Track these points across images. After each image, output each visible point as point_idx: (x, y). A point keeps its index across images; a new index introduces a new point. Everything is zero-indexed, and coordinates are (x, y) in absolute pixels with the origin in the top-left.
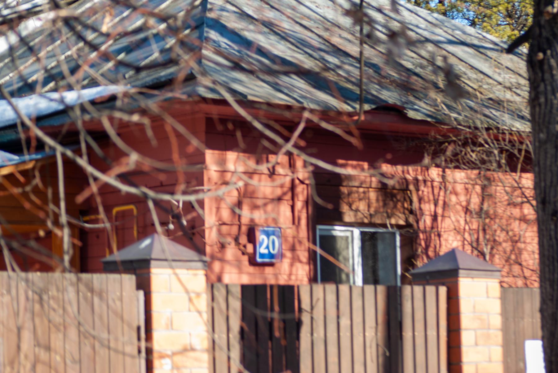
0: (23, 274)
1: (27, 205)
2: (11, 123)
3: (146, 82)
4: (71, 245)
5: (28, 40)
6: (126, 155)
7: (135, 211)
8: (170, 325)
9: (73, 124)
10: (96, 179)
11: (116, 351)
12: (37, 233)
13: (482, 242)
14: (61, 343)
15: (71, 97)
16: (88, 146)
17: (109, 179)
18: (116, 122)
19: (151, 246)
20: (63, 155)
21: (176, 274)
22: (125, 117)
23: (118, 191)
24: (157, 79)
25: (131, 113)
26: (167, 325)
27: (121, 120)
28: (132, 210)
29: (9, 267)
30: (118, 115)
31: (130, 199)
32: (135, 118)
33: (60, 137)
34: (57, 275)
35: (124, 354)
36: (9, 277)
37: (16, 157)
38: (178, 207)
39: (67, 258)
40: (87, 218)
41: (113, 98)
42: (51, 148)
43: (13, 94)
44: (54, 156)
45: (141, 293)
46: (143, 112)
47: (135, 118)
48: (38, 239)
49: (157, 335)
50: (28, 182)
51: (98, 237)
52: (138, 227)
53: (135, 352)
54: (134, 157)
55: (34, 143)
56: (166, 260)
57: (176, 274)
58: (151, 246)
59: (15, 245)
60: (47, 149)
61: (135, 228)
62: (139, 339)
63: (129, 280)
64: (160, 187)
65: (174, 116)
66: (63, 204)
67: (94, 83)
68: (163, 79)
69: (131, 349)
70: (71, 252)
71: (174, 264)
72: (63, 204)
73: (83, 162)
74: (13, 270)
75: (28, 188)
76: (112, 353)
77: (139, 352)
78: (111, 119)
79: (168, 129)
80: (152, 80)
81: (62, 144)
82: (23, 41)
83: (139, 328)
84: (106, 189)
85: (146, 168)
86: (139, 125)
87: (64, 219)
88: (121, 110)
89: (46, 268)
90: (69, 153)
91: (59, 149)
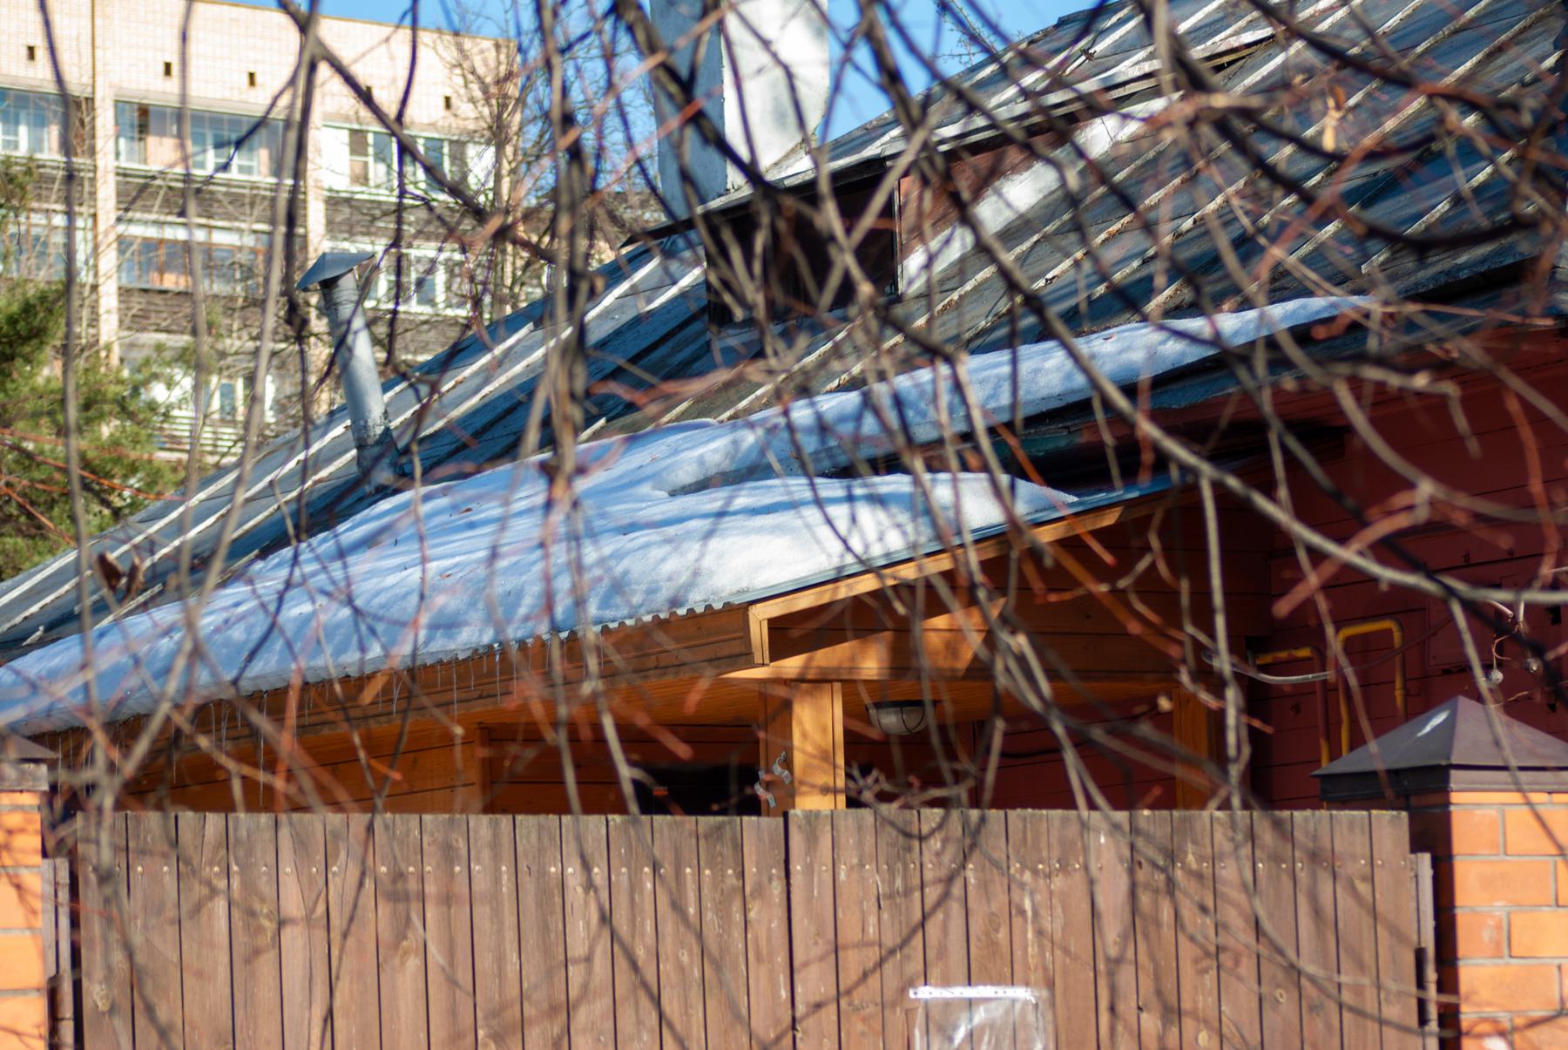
0: (1121, 816)
1: (1134, 628)
2: (1076, 398)
3: (1417, 284)
4: (1244, 732)
5: (1111, 168)
6: (1410, 486)
7: (1397, 637)
8: (1505, 945)
9: (1247, 397)
10: (1317, 556)
11: (1359, 1012)
12: (1155, 706)
13: (983, 585)
14: (1212, 1000)
15: (1232, 324)
16: (1290, 460)
17: (1348, 554)
18: (1368, 391)
19: (1449, 726)
20: (1219, 488)
21: (1529, 803)
22: (1394, 380)
23: (1374, 580)
24: (1448, 273)
25: (1411, 371)
26: (1498, 944)
27: (1380, 386)
28: (1389, 632)
29: (1081, 800)
30: (1372, 373)
31: (1402, 603)
32: (1421, 381)
33: (1212, 443)
34: (1210, 816)
35: (1382, 1022)
36: (1084, 825)
37: (1072, 499)
38: (1515, 618)
39: (1235, 771)
40: (1267, 659)
41: (1356, 328)
42: (1185, 469)
43: (1073, 318)
44: (1195, 489)
45: (1425, 859)
46: (1443, 368)
47: (1421, 381)
48: (1163, 721)
49: (1474, 972)
50: (1125, 566)
51: (1297, 709)
52: (1405, 680)
53: (1413, 1021)
54: (1426, 488)
55: (1147, 457)
56: (1505, 768)
57: (1529, 803)
58: (1449, 726)
59: (1097, 733)
60: (1174, 473)
61: (1398, 683)
62: (1421, 983)
63: (1391, 826)
64: (1473, 569)
65: (1520, 371)
66: (1220, 622)
67: (1282, 286)
68: (1464, 274)
69: (1401, 1010)
70: (1246, 751)
71: (1524, 776)
72: (1220, 622)
73: (1278, 511)
74: (1092, 806)
75: (1123, 583)
76: (1347, 1015)
77: (1423, 1020)
78: (1355, 384)
79: (1513, 406)
80: (1435, 277)
81: (1213, 458)
82: (1098, 171)
83: (1420, 954)
84: (1347, 582)
85: (1460, 519)
86: (1435, 405)
87: (1224, 663)
88: (1380, 361)
89: (1171, 796)
90: (1233, 482)
91: (1207, 470)
